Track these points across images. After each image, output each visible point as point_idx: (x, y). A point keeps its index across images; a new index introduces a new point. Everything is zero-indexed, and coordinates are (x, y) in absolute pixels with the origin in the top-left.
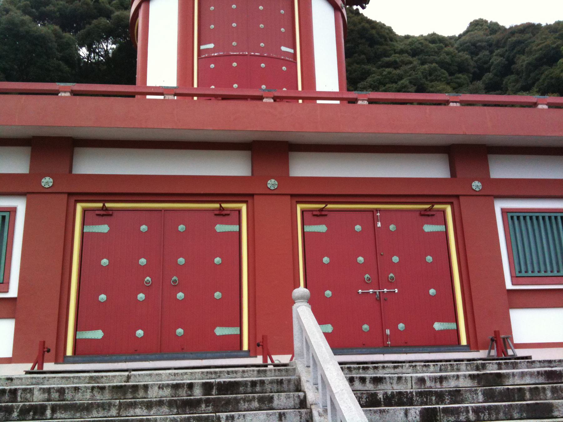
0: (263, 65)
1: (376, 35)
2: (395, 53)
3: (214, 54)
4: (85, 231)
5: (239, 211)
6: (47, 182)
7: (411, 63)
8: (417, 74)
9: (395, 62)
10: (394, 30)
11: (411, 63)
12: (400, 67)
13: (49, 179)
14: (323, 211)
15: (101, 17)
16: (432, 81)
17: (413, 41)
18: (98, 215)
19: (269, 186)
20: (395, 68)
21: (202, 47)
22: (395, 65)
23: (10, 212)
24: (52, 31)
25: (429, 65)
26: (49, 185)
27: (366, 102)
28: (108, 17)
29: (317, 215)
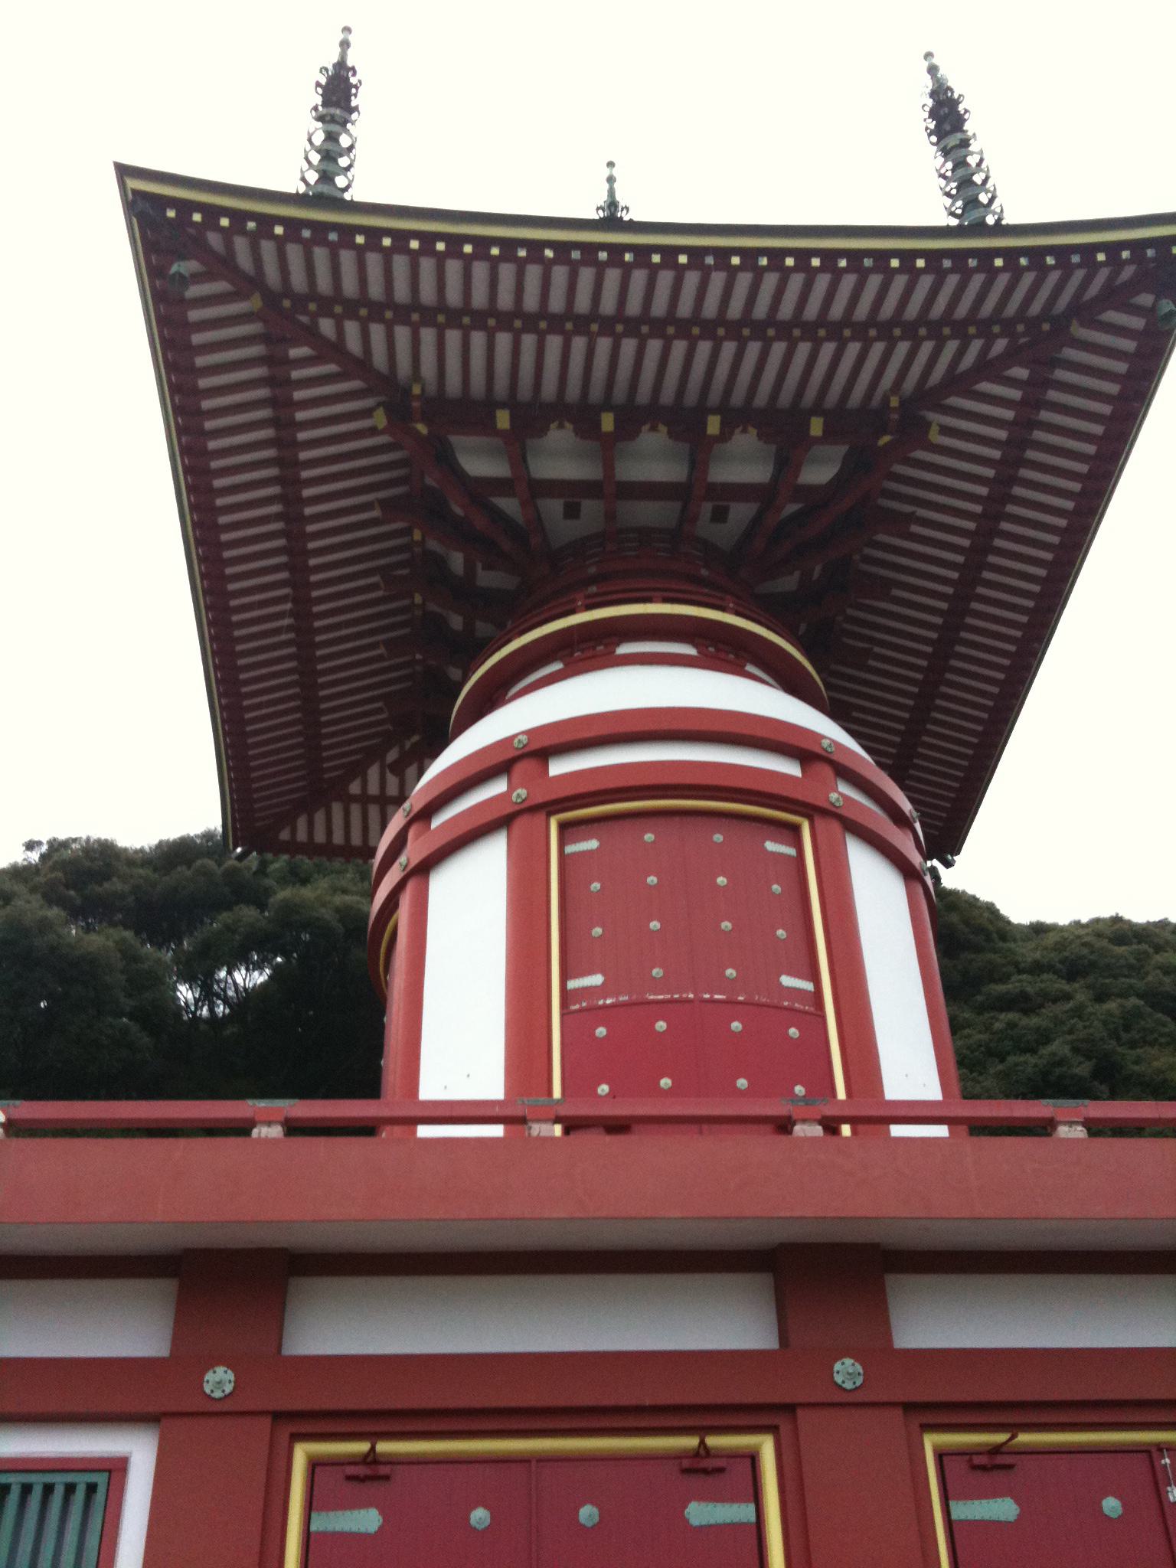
0: (736, 1026)
1: (962, 926)
2: (1020, 972)
3: (605, 999)
4: (313, 1528)
5: (753, 1459)
6: (219, 1383)
7: (1067, 997)
8: (1090, 1027)
9: (1024, 996)
10: (1002, 912)
11: (1067, 997)
12: (1040, 1008)
13: (226, 1372)
14: (1002, 1453)
15: (242, 906)
16: (1133, 1045)
17: (1066, 939)
18: (349, 1478)
19: (838, 1379)
20: (1026, 1012)
21: (572, 984)
22: (1023, 1003)
23: (110, 1471)
24: (116, 943)
25: (1119, 1000)
26: (223, 1391)
27: (1080, 1128)
28: (262, 906)
29: (983, 1468)
